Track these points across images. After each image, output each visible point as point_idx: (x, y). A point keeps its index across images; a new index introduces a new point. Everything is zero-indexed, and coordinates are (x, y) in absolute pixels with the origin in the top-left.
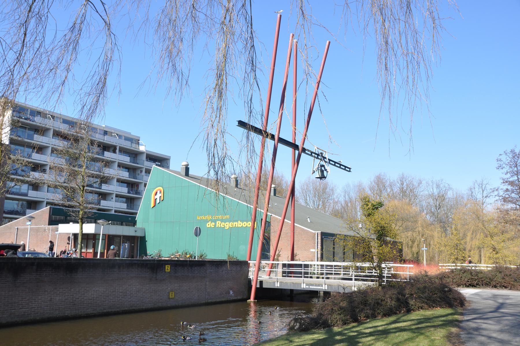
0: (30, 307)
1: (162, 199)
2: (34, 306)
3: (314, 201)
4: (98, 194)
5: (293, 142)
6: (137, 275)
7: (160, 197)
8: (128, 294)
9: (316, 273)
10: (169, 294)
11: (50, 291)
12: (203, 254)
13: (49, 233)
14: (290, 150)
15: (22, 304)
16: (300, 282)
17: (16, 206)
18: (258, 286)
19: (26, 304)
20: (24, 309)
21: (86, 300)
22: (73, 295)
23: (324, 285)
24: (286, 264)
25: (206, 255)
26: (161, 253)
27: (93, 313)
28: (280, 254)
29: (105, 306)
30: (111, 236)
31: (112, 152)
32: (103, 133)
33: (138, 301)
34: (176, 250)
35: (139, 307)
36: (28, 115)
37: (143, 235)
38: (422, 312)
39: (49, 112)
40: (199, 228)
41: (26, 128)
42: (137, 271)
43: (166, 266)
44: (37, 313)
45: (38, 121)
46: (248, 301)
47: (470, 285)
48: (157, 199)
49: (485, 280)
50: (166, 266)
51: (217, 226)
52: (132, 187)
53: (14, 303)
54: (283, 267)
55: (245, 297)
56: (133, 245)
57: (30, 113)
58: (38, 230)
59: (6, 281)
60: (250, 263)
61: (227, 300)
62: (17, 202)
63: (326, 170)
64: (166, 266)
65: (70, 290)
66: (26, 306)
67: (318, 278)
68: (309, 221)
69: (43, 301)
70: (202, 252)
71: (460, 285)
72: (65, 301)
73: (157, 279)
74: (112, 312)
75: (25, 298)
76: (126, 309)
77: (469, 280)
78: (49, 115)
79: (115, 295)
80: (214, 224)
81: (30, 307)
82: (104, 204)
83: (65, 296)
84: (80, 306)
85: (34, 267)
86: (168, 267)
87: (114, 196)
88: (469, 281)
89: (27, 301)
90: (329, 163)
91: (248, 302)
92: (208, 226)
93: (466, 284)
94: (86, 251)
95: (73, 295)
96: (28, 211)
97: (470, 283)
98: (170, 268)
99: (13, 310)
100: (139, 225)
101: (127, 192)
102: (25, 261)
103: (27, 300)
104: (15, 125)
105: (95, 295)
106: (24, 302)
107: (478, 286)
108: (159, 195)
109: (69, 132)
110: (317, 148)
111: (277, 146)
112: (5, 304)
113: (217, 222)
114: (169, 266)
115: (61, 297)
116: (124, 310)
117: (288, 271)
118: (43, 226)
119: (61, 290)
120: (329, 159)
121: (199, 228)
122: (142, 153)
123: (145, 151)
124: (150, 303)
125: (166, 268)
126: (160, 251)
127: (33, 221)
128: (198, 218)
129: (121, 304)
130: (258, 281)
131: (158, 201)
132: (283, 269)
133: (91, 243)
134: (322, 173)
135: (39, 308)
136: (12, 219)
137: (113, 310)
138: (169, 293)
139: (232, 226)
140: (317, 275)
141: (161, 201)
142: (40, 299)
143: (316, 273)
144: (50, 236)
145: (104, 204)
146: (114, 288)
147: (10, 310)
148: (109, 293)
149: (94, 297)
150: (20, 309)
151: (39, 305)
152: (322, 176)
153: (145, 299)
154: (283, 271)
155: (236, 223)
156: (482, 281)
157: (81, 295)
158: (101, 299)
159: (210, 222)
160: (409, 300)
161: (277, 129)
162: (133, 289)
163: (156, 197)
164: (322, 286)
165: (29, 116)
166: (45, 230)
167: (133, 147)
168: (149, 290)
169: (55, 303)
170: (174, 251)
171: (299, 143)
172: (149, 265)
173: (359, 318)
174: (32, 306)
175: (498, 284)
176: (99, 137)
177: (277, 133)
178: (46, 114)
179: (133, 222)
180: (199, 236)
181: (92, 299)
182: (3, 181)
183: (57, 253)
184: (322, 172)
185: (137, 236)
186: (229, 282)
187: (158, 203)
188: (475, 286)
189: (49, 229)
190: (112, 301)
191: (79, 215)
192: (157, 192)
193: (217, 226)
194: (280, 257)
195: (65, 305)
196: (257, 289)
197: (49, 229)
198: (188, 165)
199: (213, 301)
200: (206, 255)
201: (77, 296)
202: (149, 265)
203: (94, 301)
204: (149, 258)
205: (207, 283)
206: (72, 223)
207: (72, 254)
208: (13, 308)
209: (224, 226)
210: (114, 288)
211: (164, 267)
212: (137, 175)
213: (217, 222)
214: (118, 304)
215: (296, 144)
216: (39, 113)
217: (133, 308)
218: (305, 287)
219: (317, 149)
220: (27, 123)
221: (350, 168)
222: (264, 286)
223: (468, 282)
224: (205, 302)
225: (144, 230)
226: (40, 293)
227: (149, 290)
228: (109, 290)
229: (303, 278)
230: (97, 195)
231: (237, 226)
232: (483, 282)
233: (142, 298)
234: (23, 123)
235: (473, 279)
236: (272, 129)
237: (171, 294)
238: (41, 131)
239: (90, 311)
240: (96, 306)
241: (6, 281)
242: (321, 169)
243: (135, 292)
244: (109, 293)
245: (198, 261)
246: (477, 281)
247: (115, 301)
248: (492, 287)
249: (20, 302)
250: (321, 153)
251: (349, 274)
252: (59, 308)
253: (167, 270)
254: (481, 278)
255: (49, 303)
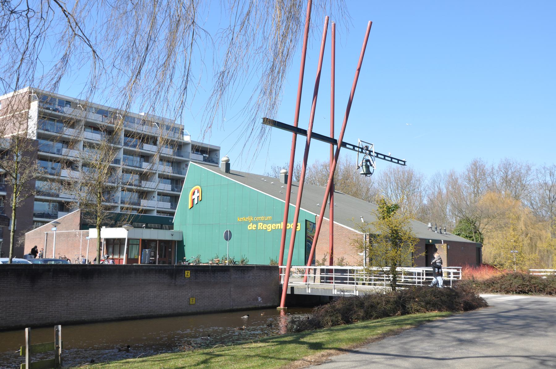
0: (48, 311)
1: (200, 199)
2: (52, 310)
3: (397, 195)
4: (170, 179)
5: (332, 137)
6: (155, 280)
7: (198, 197)
8: (146, 299)
9: (364, 279)
10: (190, 300)
11: (67, 296)
12: (245, 259)
13: (80, 238)
14: (327, 146)
15: (40, 308)
16: (331, 288)
17: (47, 207)
18: (289, 292)
19: (44, 308)
20: (42, 312)
21: (103, 305)
22: (89, 301)
23: (355, 291)
24: (324, 269)
25: (247, 260)
26: (200, 258)
27: (109, 318)
28: (326, 258)
29: (122, 311)
30: (146, 241)
31: (153, 144)
32: (141, 122)
33: (156, 307)
34: (216, 255)
35: (157, 313)
36: (57, 106)
37: (181, 239)
38: (418, 315)
39: (80, 100)
40: (230, 231)
41: (54, 120)
42: (155, 277)
43: (186, 272)
44: (55, 317)
45: (68, 111)
46: (277, 308)
47: (521, 291)
48: (194, 199)
49: (538, 286)
50: (186, 272)
51: (259, 228)
52: (177, 184)
53: (33, 307)
54: (321, 273)
55: (276, 304)
56: (170, 250)
57: (59, 103)
58: (68, 235)
59: (24, 287)
60: (282, 269)
61: (254, 307)
62: (48, 203)
63: (371, 165)
64: (186, 272)
65: (86, 295)
66: (43, 310)
67: (364, 284)
68: (363, 221)
69: (60, 306)
70: (243, 257)
71: (510, 292)
72: (81, 306)
73: (176, 285)
74: (129, 317)
75: (42, 303)
76: (144, 314)
77: (520, 285)
78: (79, 104)
79: (132, 300)
80: (255, 226)
81: (48, 311)
82: (145, 204)
83: (81, 301)
84: (97, 310)
85: (51, 273)
86: (188, 272)
87: (156, 195)
88: (520, 287)
89: (45, 306)
90: (377, 157)
91: (277, 309)
92: (249, 228)
93: (516, 290)
94: (119, 257)
95: (89, 301)
96: (60, 213)
97: (520, 289)
98: (190, 274)
99: (32, 313)
100: (176, 228)
101: (170, 190)
102: (41, 268)
103: (44, 305)
104: (42, 116)
105: (111, 301)
106: (42, 307)
107: (530, 293)
108: (196, 195)
109: (103, 123)
110: (361, 141)
111: (310, 143)
112: (24, 308)
113: (259, 224)
114: (189, 272)
115: (77, 302)
116: (142, 316)
117: (326, 277)
118: (74, 231)
119: (77, 295)
120: (375, 153)
121: (230, 231)
122: (186, 144)
123: (190, 141)
124: (169, 309)
125: (186, 273)
126: (199, 257)
127: (59, 226)
128: (238, 219)
129: (139, 310)
130: (289, 288)
131: (196, 201)
132: (321, 275)
133: (117, 248)
134: (367, 169)
135: (56, 312)
136: (44, 223)
137: (130, 316)
138: (189, 299)
139: (274, 228)
140: (365, 281)
141: (199, 201)
142: (57, 304)
143: (364, 279)
144: (81, 241)
145: (145, 204)
146: (131, 294)
147: (29, 313)
148: (125, 299)
149: (110, 303)
150: (38, 312)
151: (56, 309)
152: (367, 172)
153: (163, 305)
154: (321, 277)
155: (279, 225)
156: (535, 287)
157: (97, 300)
158: (118, 304)
159: (251, 224)
160: (407, 303)
161: (309, 124)
162: (151, 295)
163: (194, 197)
164: (353, 292)
165: (57, 107)
166: (76, 235)
167: (176, 137)
168: (167, 295)
169: (71, 307)
170: (214, 256)
171: (337, 137)
172: (167, 270)
173: (350, 320)
174: (50, 310)
175: (553, 290)
176: (136, 128)
177: (309, 128)
178: (77, 104)
179: (171, 226)
180: (229, 240)
181: (108, 305)
182: (20, 191)
183: (88, 260)
184: (367, 167)
185: (174, 240)
186: (257, 289)
187: (197, 204)
188: (528, 293)
189: (80, 234)
190: (129, 306)
191: (96, 222)
192: (194, 192)
193: (259, 228)
194: (326, 262)
195: (82, 310)
196: (287, 295)
197: (80, 234)
198: (228, 160)
199: (238, 308)
200: (247, 260)
201: (94, 301)
202: (167, 270)
203: (110, 306)
204: (186, 263)
205: (232, 289)
206: (105, 227)
207: (104, 261)
208: (32, 312)
209: (266, 228)
210: (131, 294)
211: (183, 272)
212: (182, 170)
213: (259, 224)
214: (135, 310)
215: (335, 138)
216: (68, 103)
217: (151, 314)
218: (336, 293)
219: (360, 142)
220: (55, 115)
221: (404, 162)
222: (296, 292)
223: (519, 288)
224: (229, 308)
225: (181, 234)
226: (57, 298)
227: (167, 295)
228: (125, 296)
229: (334, 284)
230: (170, 181)
231: (280, 228)
232: (536, 288)
233: (161, 303)
234: (50, 115)
235: (524, 285)
236: (303, 125)
237: (191, 300)
238: (72, 124)
239: (106, 316)
240: (113, 311)
241: (24, 287)
242: (367, 164)
243: (153, 297)
244: (125, 299)
245: (56, 265)
246: (529, 287)
247: (132, 307)
248: (547, 294)
249: (38, 306)
250: (366, 146)
251: (401, 280)
252: (76, 312)
253: (187, 275)
254: (534, 284)
255: (65, 308)
